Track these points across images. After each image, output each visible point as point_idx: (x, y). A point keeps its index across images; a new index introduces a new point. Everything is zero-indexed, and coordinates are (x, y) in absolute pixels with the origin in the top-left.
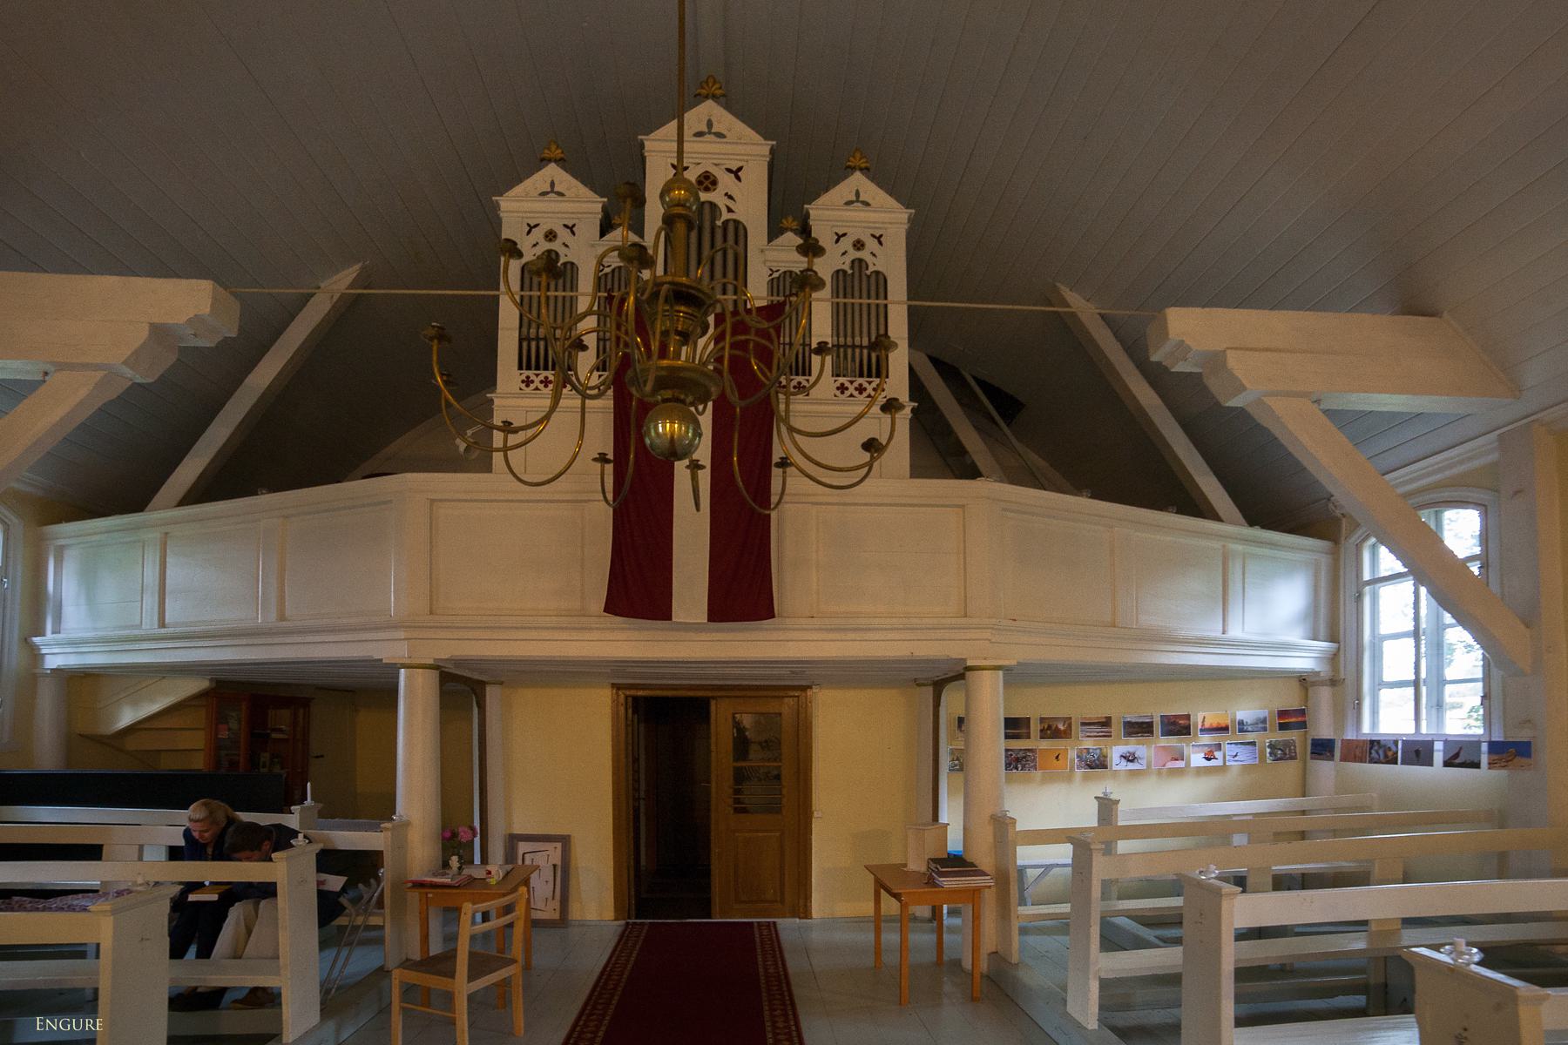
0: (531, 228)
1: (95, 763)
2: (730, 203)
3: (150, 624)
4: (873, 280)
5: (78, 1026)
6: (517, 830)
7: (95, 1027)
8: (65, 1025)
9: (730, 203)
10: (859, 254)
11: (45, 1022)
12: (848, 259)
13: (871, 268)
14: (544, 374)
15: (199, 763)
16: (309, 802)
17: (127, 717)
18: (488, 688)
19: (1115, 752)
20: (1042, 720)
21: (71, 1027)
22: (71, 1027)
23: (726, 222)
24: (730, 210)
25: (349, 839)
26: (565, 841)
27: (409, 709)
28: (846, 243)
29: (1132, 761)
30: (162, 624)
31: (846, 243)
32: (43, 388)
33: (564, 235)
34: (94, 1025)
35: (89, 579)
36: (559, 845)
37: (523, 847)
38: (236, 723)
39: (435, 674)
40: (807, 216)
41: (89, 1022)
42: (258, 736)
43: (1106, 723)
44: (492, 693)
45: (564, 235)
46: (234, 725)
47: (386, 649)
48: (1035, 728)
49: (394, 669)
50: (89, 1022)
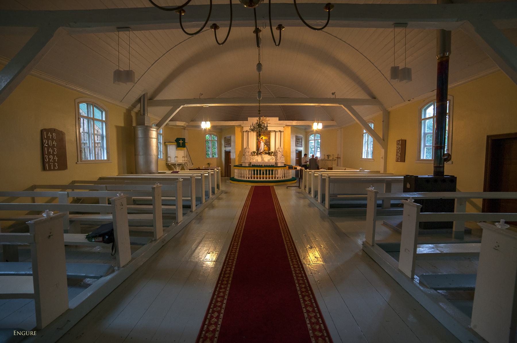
5: (28, 334)
11: (17, 333)
21: (26, 334)
22: (26, 334)
34: (33, 333)
41: (32, 332)
50: (32, 332)
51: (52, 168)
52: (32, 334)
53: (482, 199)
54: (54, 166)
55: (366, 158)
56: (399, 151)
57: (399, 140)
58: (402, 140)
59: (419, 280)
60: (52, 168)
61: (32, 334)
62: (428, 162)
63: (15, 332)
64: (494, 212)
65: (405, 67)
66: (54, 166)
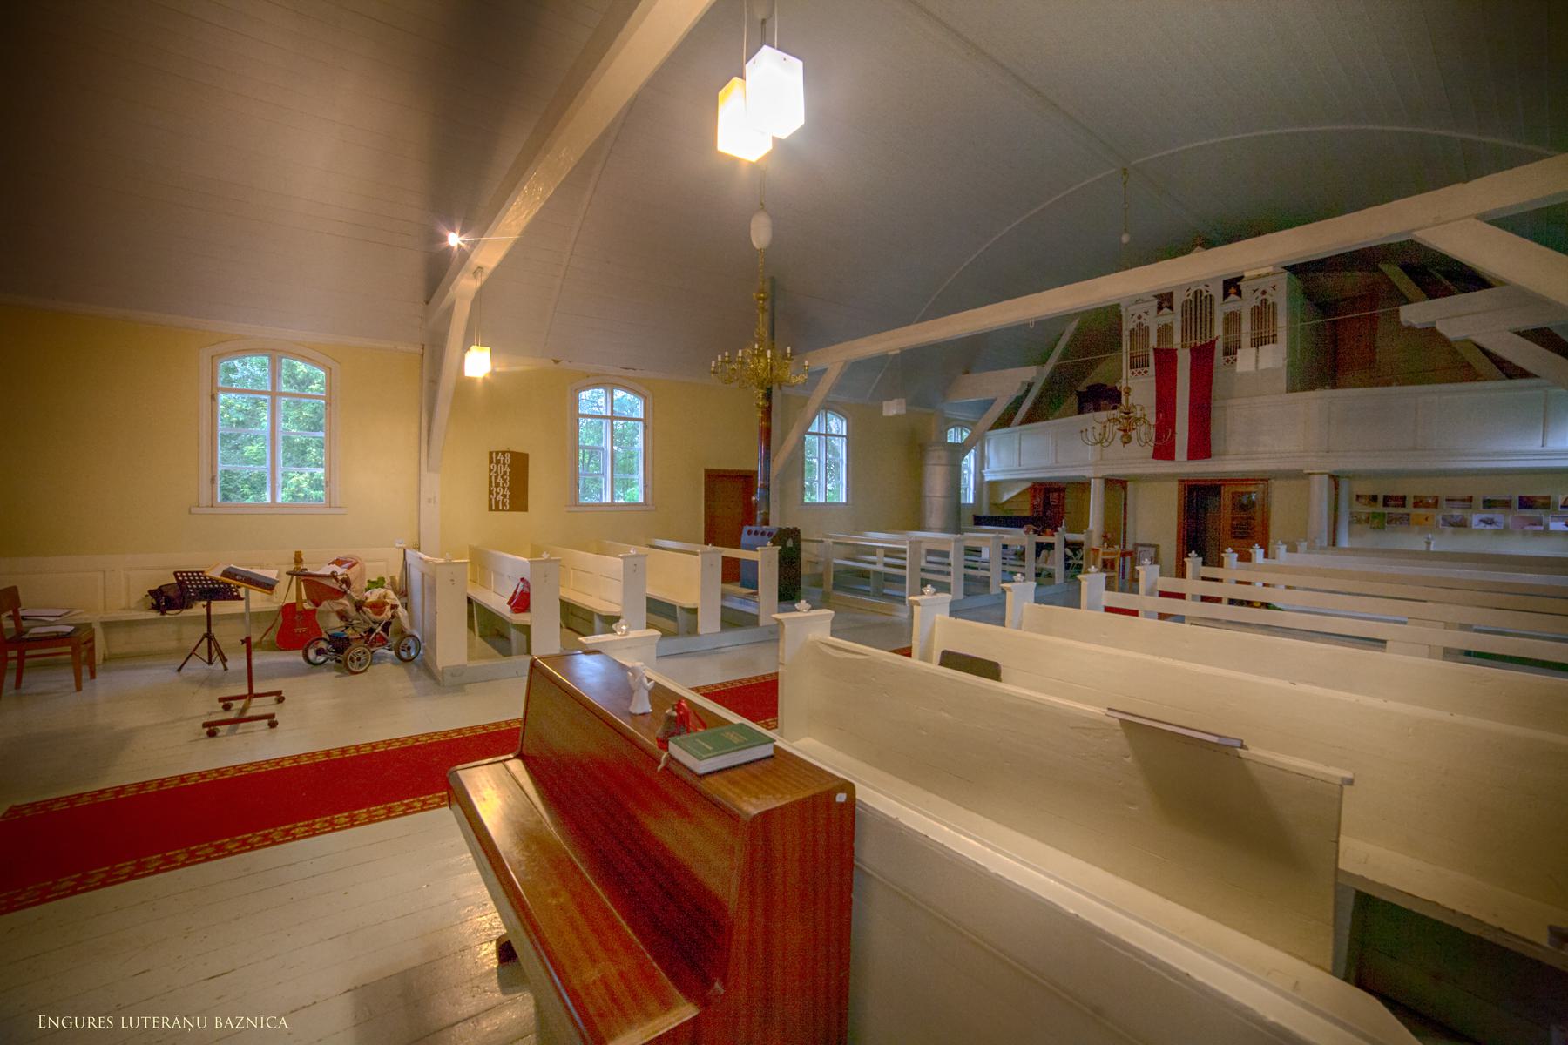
0: (1133, 315)
1: (998, 513)
2: (1207, 288)
3: (1016, 466)
4: (1271, 307)
5: (80, 1024)
6: (1139, 542)
7: (97, 1025)
8: (67, 1022)
9: (1207, 288)
10: (1264, 297)
12: (1259, 300)
13: (1205, 294)
14: (1139, 369)
15: (1027, 514)
16: (1063, 527)
17: (1006, 497)
18: (1129, 483)
19: (1475, 519)
20: (1415, 497)
21: (74, 1025)
22: (74, 1025)
23: (1206, 297)
24: (1207, 291)
25: (1073, 537)
26: (1157, 547)
27: (1094, 491)
28: (1258, 293)
29: (1491, 524)
30: (1020, 465)
31: (1258, 293)
32: (511, 449)
33: (1144, 316)
34: (97, 1023)
35: (997, 452)
36: (1154, 549)
37: (1140, 549)
38: (1039, 500)
39: (1103, 481)
40: (1239, 286)
41: (91, 1020)
42: (1046, 504)
43: (1470, 499)
44: (1130, 485)
45: (1144, 316)
46: (1039, 500)
47: (1087, 473)
48: (1410, 502)
49: (1090, 479)
50: (91, 1020)
51: (501, 508)
52: (91, 1025)
53: (761, 625)
54: (504, 504)
55: (609, 501)
56: (505, 482)
57: (503, 453)
58: (514, 455)
59: (1201, 345)
60: (501, 508)
61: (91, 1025)
62: (628, 508)
63: (42, 1018)
64: (871, 646)
65: (845, 439)
66: (504, 504)
